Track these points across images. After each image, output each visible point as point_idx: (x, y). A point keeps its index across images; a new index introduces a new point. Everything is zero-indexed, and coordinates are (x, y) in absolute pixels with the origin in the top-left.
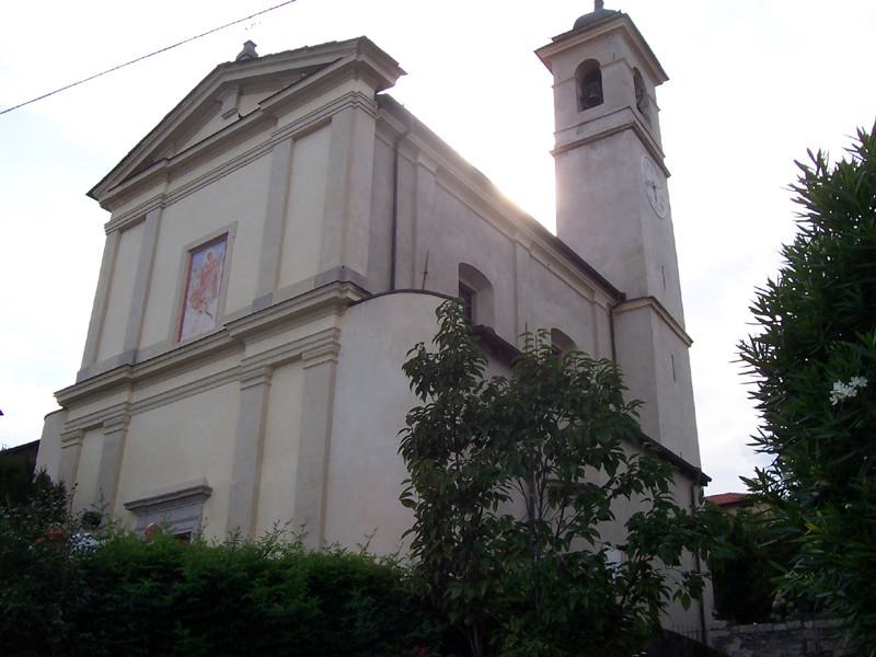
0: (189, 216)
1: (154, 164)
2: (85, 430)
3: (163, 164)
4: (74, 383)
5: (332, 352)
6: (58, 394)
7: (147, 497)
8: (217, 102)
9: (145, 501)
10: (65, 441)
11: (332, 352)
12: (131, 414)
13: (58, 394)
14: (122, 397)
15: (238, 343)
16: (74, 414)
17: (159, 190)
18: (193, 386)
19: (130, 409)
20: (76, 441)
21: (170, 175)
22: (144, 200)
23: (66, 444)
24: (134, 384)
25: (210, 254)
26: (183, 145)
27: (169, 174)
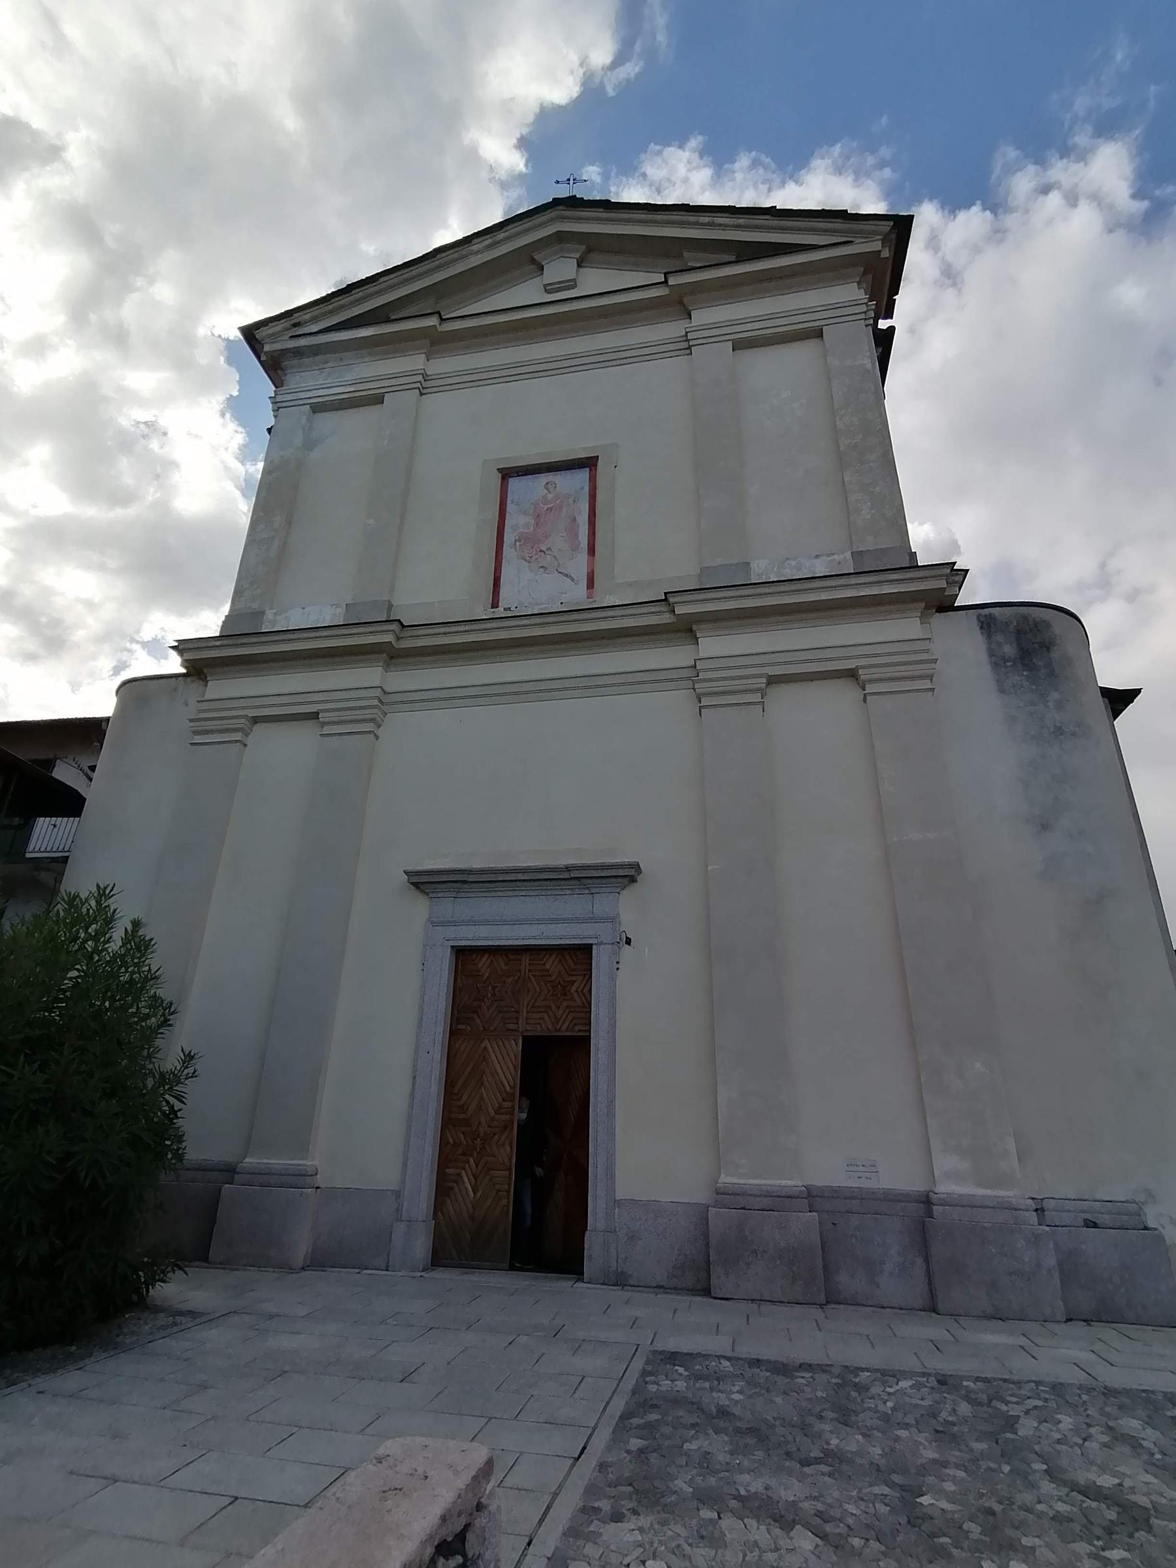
0: (481, 414)
1: (388, 321)
2: (256, 720)
3: (432, 321)
4: (215, 632)
5: (372, 720)
6: (240, 328)
7: (477, 865)
8: (533, 261)
9: (469, 872)
10: (196, 733)
11: (372, 720)
12: (384, 708)
13: (240, 328)
14: (370, 675)
15: (686, 630)
16: (220, 688)
17: (415, 362)
18: (567, 683)
19: (385, 700)
20: (238, 736)
21: (437, 343)
22: (427, 267)
23: (198, 739)
24: (393, 656)
25: (513, 502)
26: (477, 298)
27: (432, 344)
